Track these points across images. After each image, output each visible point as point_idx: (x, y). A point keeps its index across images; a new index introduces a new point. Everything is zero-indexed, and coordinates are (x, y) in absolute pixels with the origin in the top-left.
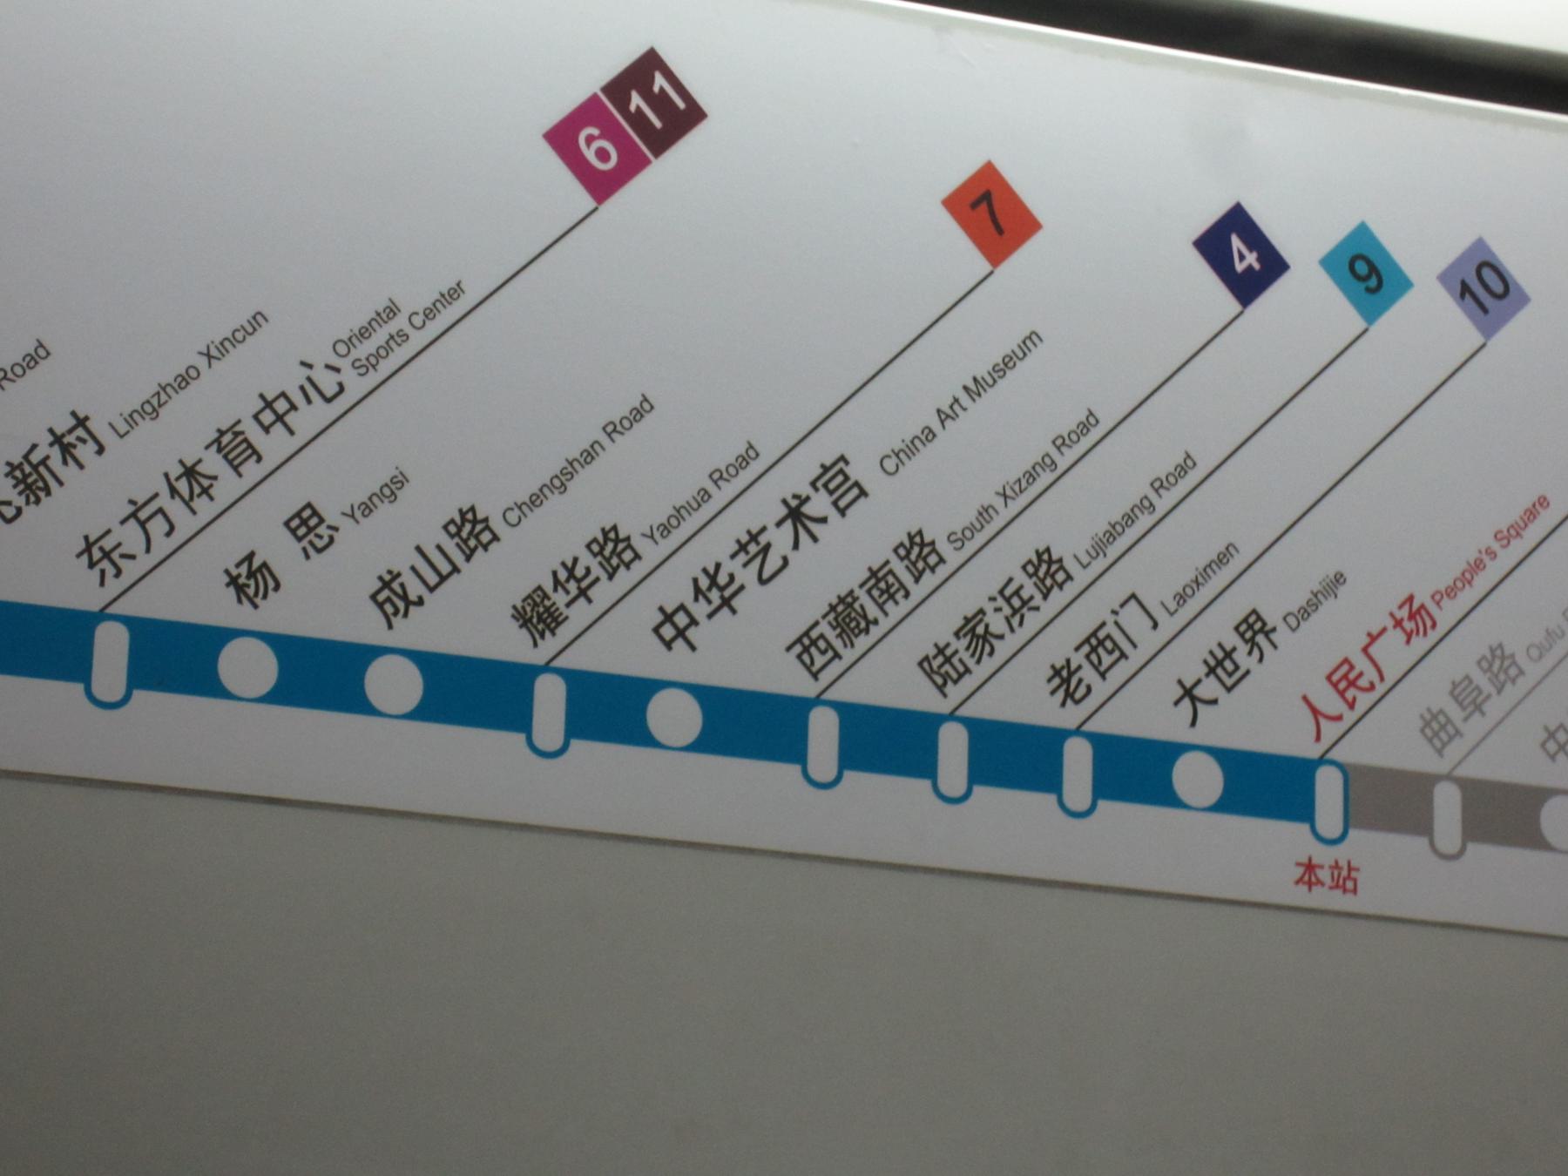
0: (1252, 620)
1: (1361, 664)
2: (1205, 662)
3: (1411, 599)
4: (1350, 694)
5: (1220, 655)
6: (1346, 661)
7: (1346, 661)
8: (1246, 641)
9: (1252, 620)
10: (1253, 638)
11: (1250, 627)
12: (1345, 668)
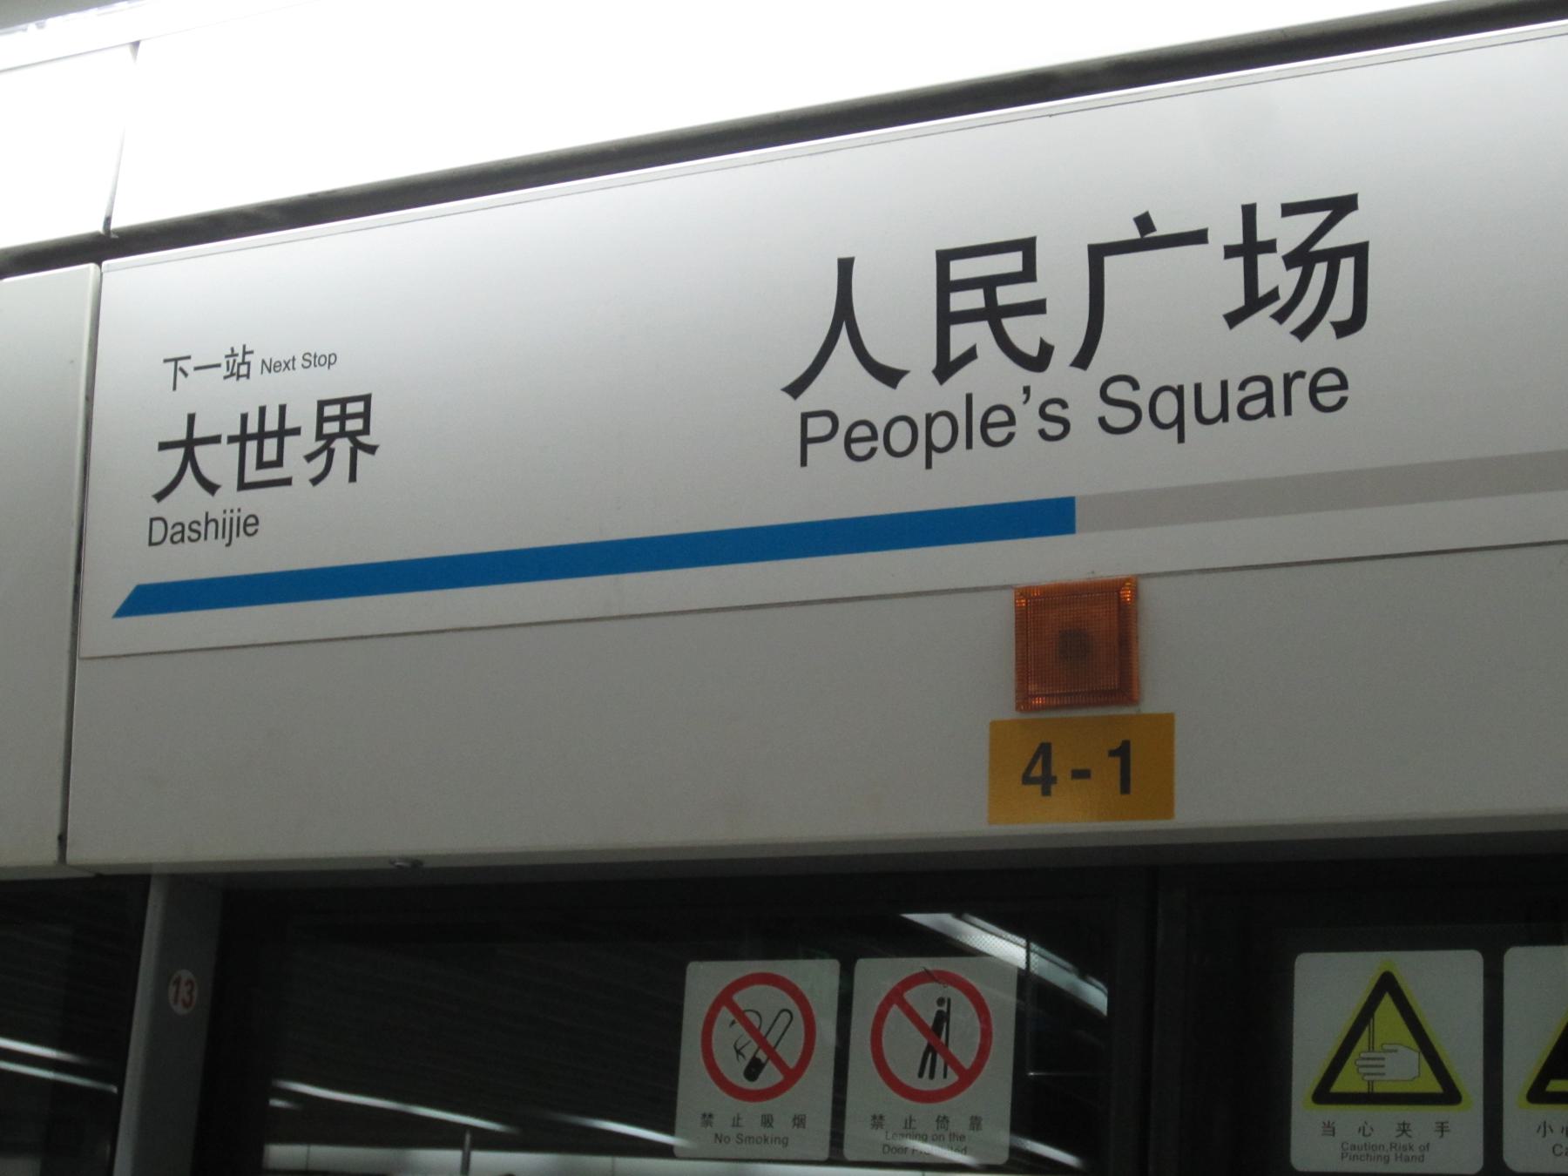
0: (353, 408)
2: (244, 418)
3: (1342, 206)
4: (962, 337)
5: (272, 424)
6: (1027, 247)
7: (1027, 247)
8: (320, 435)
9: (353, 408)
10: (331, 438)
11: (343, 417)
12: (1012, 262)
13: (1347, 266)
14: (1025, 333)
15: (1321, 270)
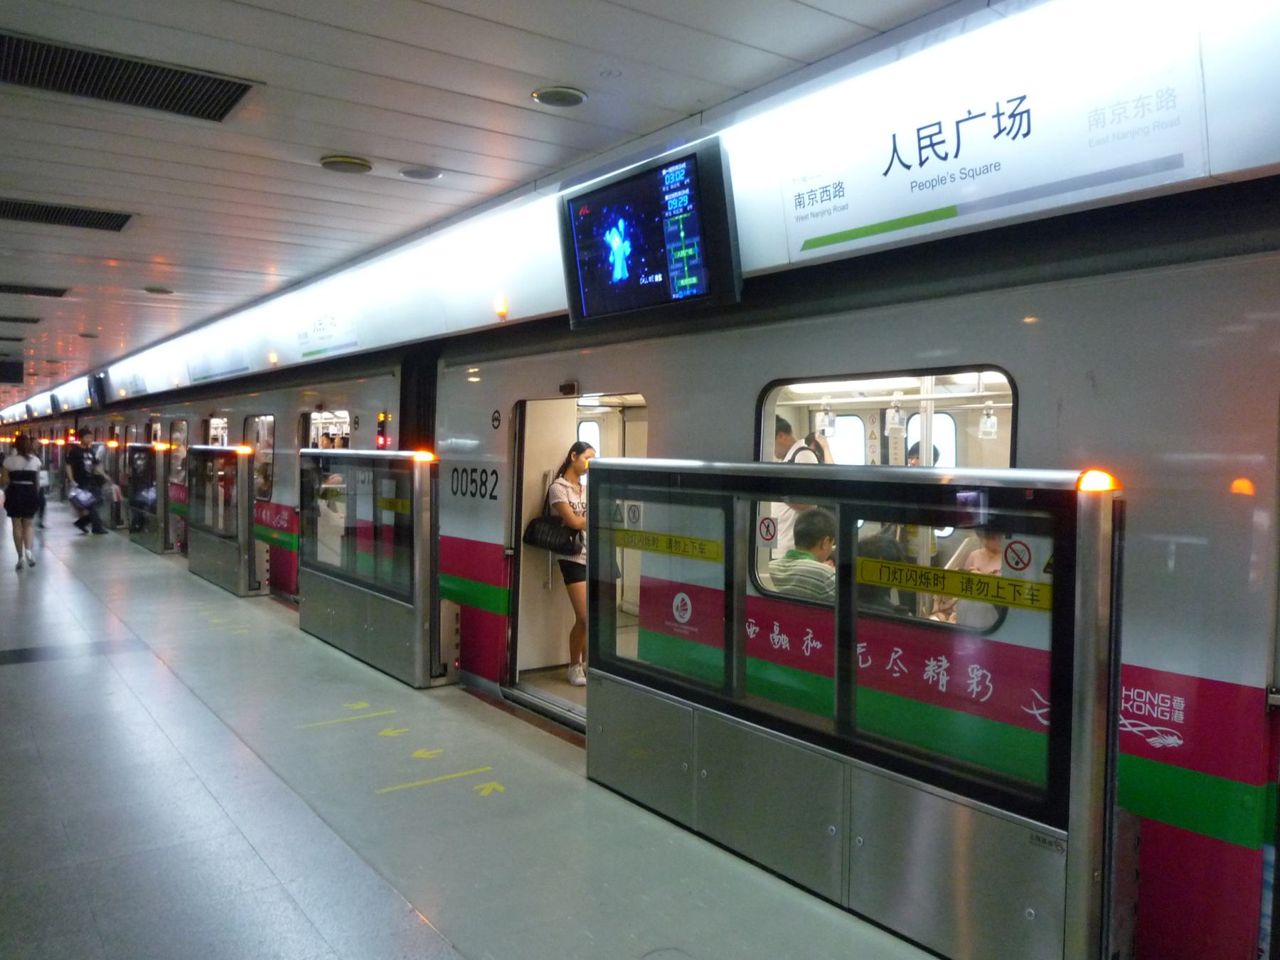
1: (949, 134)
3: (1023, 98)
12: (936, 129)
13: (1025, 116)
14: (941, 150)
15: (1018, 118)
